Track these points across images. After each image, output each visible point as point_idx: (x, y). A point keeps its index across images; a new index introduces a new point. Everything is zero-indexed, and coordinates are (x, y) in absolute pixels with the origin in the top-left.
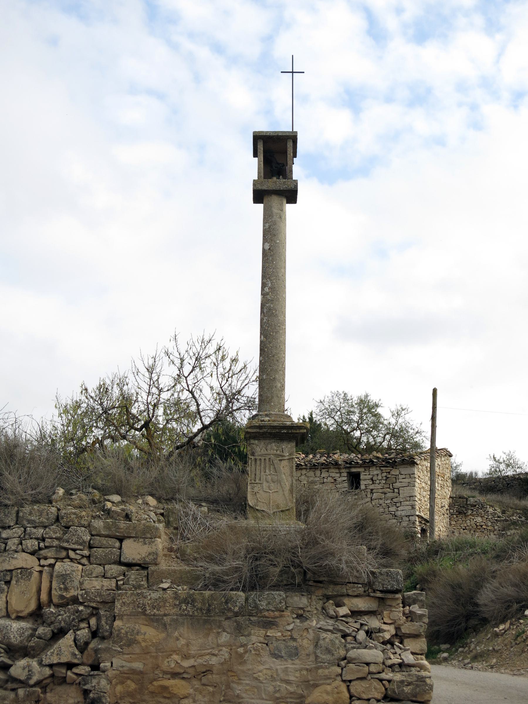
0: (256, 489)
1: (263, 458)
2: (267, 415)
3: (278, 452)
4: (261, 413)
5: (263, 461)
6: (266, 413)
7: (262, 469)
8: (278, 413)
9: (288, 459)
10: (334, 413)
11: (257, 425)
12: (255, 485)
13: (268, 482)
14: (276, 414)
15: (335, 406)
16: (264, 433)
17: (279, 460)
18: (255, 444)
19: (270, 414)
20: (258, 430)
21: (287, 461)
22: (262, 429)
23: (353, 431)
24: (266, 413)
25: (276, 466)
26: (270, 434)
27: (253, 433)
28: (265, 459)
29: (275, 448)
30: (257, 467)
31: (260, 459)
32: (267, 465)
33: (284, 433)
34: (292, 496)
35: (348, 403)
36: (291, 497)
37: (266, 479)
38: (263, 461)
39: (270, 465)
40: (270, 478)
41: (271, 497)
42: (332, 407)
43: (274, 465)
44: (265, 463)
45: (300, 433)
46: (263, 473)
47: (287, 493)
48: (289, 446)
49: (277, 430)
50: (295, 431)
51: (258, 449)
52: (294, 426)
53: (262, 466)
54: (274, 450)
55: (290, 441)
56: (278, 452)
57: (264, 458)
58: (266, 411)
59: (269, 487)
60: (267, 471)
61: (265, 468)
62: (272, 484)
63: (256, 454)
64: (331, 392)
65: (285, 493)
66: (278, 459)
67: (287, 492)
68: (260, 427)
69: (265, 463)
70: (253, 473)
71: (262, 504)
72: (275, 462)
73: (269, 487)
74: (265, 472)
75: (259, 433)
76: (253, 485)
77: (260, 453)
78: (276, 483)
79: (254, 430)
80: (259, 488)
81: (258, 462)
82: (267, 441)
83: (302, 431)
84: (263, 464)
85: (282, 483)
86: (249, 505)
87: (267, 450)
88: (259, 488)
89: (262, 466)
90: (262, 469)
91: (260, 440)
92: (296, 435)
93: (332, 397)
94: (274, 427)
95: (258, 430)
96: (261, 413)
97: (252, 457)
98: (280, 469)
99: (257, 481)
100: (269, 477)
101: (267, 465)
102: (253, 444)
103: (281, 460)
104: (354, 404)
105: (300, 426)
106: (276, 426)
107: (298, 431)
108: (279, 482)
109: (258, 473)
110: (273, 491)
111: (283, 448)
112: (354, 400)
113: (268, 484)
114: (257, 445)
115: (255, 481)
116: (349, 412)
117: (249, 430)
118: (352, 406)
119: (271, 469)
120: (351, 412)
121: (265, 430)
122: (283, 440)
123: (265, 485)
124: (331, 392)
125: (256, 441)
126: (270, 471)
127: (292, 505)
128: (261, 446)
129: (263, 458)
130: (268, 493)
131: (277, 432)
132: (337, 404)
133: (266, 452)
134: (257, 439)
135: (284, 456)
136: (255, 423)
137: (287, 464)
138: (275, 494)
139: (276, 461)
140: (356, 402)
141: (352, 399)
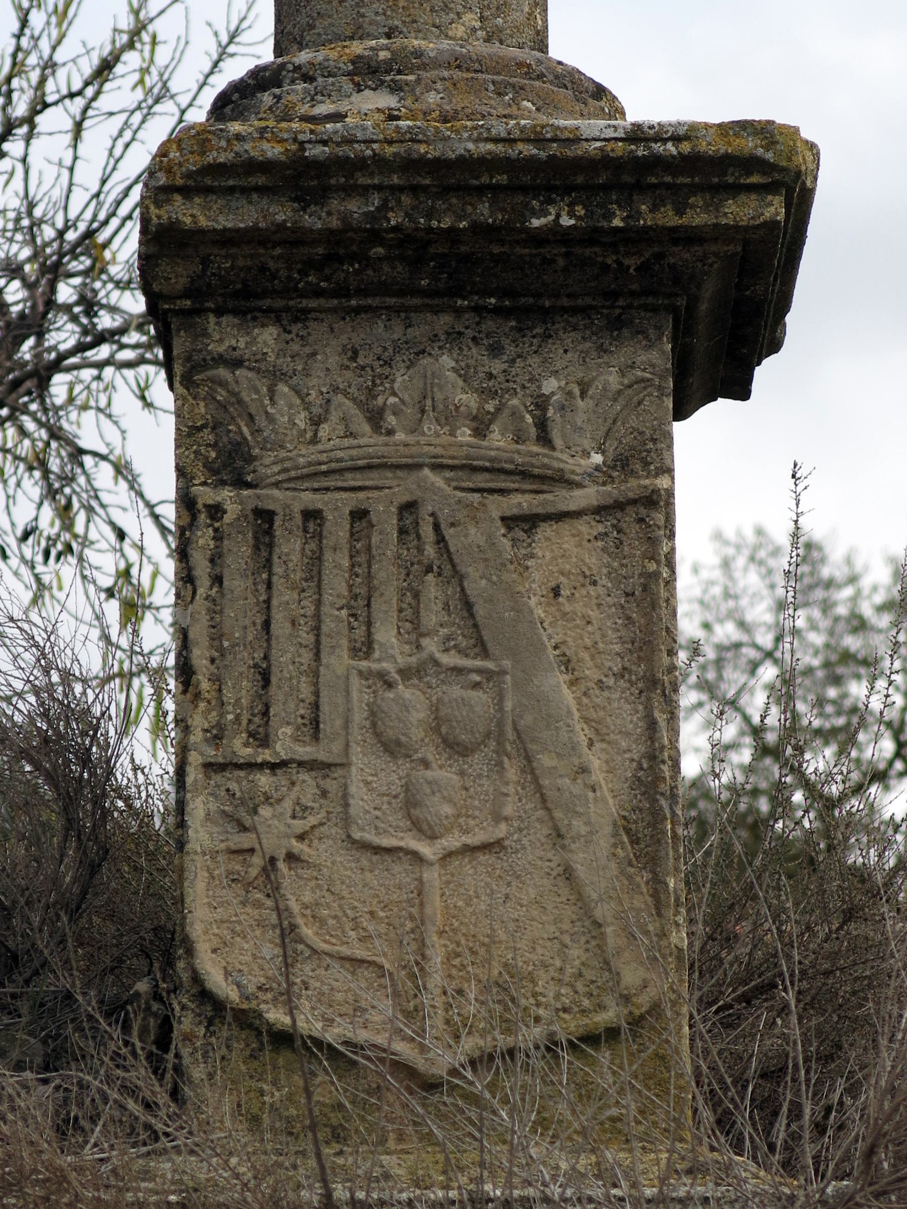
0: (275, 828)
1: (336, 507)
2: (367, 73)
3: (498, 440)
4: (304, 57)
5: (338, 529)
6: (357, 48)
7: (335, 619)
8: (479, 47)
9: (600, 511)
10: (734, 678)
11: (273, 151)
12: (264, 780)
13: (392, 748)
14: (458, 62)
15: (742, 625)
16: (341, 246)
17: (510, 521)
18: (258, 364)
19: (415, 61)
20: (282, 213)
21: (586, 527)
22: (321, 195)
23: (859, 789)
24: (357, 48)
25: (476, 585)
26: (413, 246)
27: (228, 239)
28: (359, 515)
29: (468, 400)
30: (283, 596)
31: (312, 515)
32: (387, 574)
33: (555, 234)
34: (657, 885)
35: (827, 606)
36: (642, 901)
37: (373, 714)
38: (338, 529)
39: (414, 573)
40: (419, 714)
41: (435, 904)
42: (727, 632)
43: (459, 577)
44: (362, 557)
45: (721, 233)
46: (338, 661)
47: (598, 857)
48: (613, 380)
49: (484, 211)
50: (668, 218)
51: (286, 413)
52: (657, 163)
53: (336, 584)
54: (449, 417)
55: (617, 325)
56: (498, 440)
57: (347, 502)
58: (359, 34)
59: (410, 802)
60: (386, 635)
61: (361, 607)
62: (444, 774)
63: (267, 466)
64: (718, 536)
65: (579, 860)
66: (498, 506)
67: (603, 842)
68: (302, 178)
69: (362, 557)
70: (242, 662)
71: (338, 976)
72: (467, 538)
73: (410, 802)
74: (364, 648)
75: (292, 238)
76: (235, 782)
77: (306, 455)
78: (477, 763)
79: (242, 215)
80: (301, 810)
81: (290, 547)
82: (381, 333)
83: (740, 211)
84: (336, 562)
85: (546, 761)
86: (205, 995)
87: (375, 418)
88: (301, 810)
89: (336, 584)
90: (335, 619)
91: (301, 316)
92: (681, 256)
93: (726, 564)
94: (452, 177)
95: (282, 213)
96: (304, 57)
97: (226, 495)
98: (520, 609)
99: (285, 743)
100: (412, 705)
101: (387, 574)
102: (237, 363)
103: (525, 523)
104: (866, 610)
105: (725, 162)
106: (466, 163)
107: (698, 217)
108: (513, 744)
109: (288, 656)
110: (453, 841)
111: (541, 404)
112: (866, 583)
113: (392, 775)
114: (276, 376)
115: (262, 739)
116: (841, 664)
117: (190, 213)
118: (859, 625)
119: (432, 616)
120: (847, 657)
121: (355, 208)
122: (546, 315)
123: (369, 780)
124: (718, 536)
125: (267, 338)
126: (414, 628)
127: (653, 974)
128: (316, 386)
129: (336, 507)
130: (400, 871)
131: (479, 230)
132: (761, 613)
133: (370, 442)
134: (275, 316)
135: (562, 480)
136: (259, 138)
137: (593, 560)
138: (470, 872)
139: (475, 534)
140: (879, 599)
141: (853, 579)
